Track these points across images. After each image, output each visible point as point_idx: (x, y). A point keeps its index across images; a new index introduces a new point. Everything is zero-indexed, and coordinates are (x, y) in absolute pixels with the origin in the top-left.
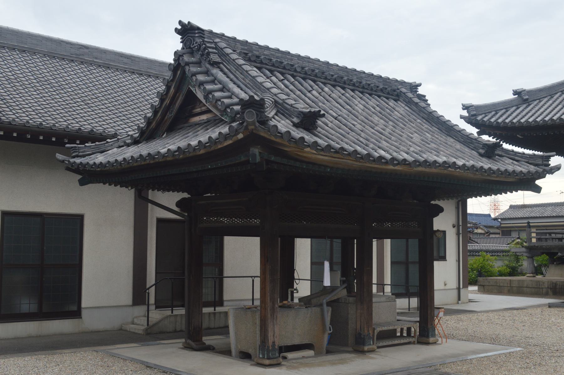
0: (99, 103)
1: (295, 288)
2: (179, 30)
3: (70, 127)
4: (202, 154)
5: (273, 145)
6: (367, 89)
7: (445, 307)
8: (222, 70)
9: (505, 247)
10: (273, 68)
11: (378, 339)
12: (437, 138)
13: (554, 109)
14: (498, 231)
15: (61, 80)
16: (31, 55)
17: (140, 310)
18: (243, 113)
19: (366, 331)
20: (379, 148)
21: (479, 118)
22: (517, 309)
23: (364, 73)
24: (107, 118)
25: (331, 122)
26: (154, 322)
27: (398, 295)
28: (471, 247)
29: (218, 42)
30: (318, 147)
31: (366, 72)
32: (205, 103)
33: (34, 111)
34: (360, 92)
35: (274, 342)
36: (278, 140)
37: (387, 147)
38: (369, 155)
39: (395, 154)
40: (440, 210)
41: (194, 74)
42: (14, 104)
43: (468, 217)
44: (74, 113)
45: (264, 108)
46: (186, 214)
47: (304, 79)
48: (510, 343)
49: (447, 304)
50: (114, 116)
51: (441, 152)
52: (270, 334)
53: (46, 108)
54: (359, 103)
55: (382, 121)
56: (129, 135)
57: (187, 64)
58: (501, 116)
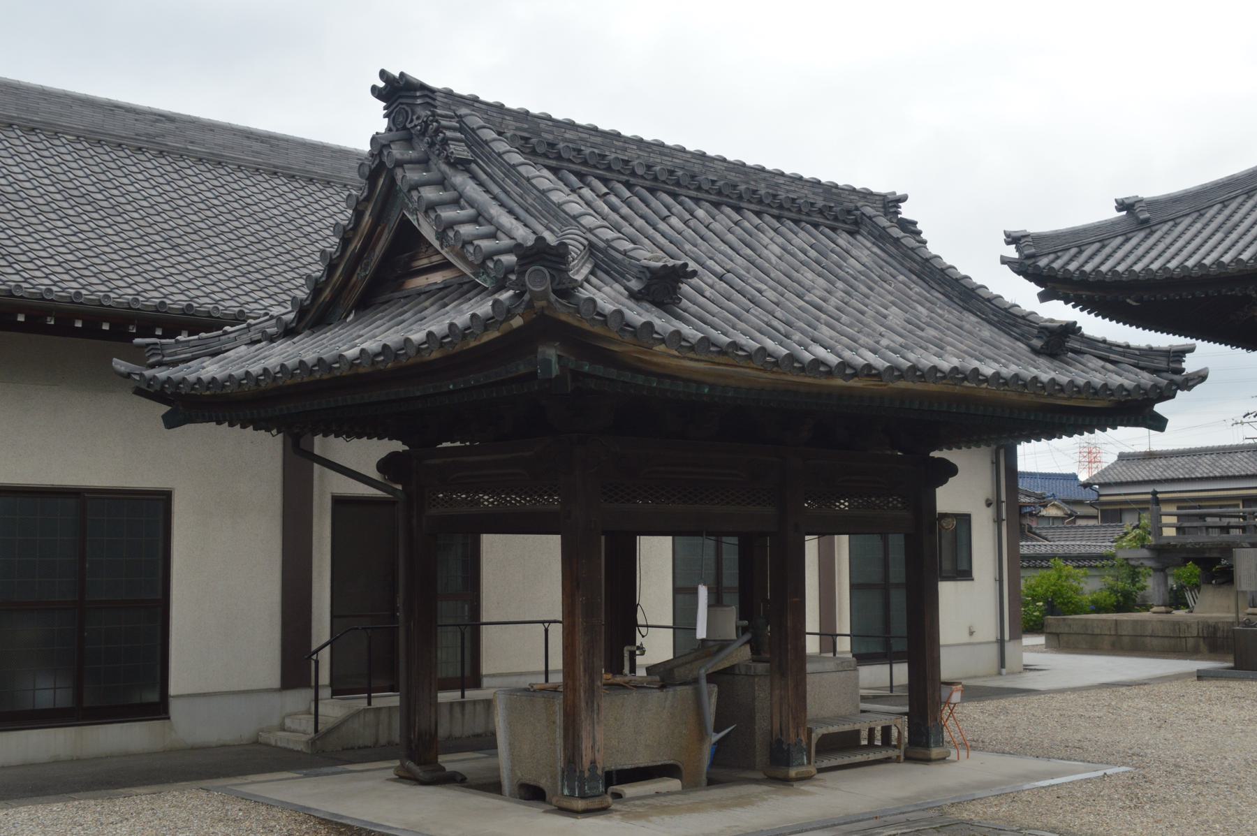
0: (203, 244)
1: (638, 644)
2: (380, 90)
3: (141, 299)
4: (436, 360)
5: (587, 339)
6: (789, 210)
7: (964, 682)
8: (474, 177)
9: (1103, 546)
10: (584, 169)
11: (818, 752)
12: (941, 316)
13: (1206, 242)
14: (1092, 511)
15: (115, 192)
16: (48, 138)
17: (299, 699)
18: (521, 274)
19: (792, 735)
20: (814, 340)
21: (1043, 262)
22: (1129, 685)
23: (782, 174)
24: (221, 277)
25: (712, 287)
26: (330, 726)
27: (863, 658)
28: (1026, 548)
29: (466, 115)
30: (683, 343)
31: (787, 172)
32: (439, 248)
33: (60, 264)
34: (773, 216)
35: (593, 762)
36: (597, 329)
37: (831, 338)
38: (792, 357)
39: (847, 354)
40: (949, 470)
41: (415, 187)
42: (16, 250)
44: (148, 267)
45: (566, 263)
46: (400, 487)
47: (652, 191)
49: (975, 677)
50: (236, 273)
51: (949, 348)
52: (586, 744)
53: (86, 257)
54: (773, 242)
55: (821, 281)
56: (272, 317)
57: (400, 164)
58: (1091, 257)
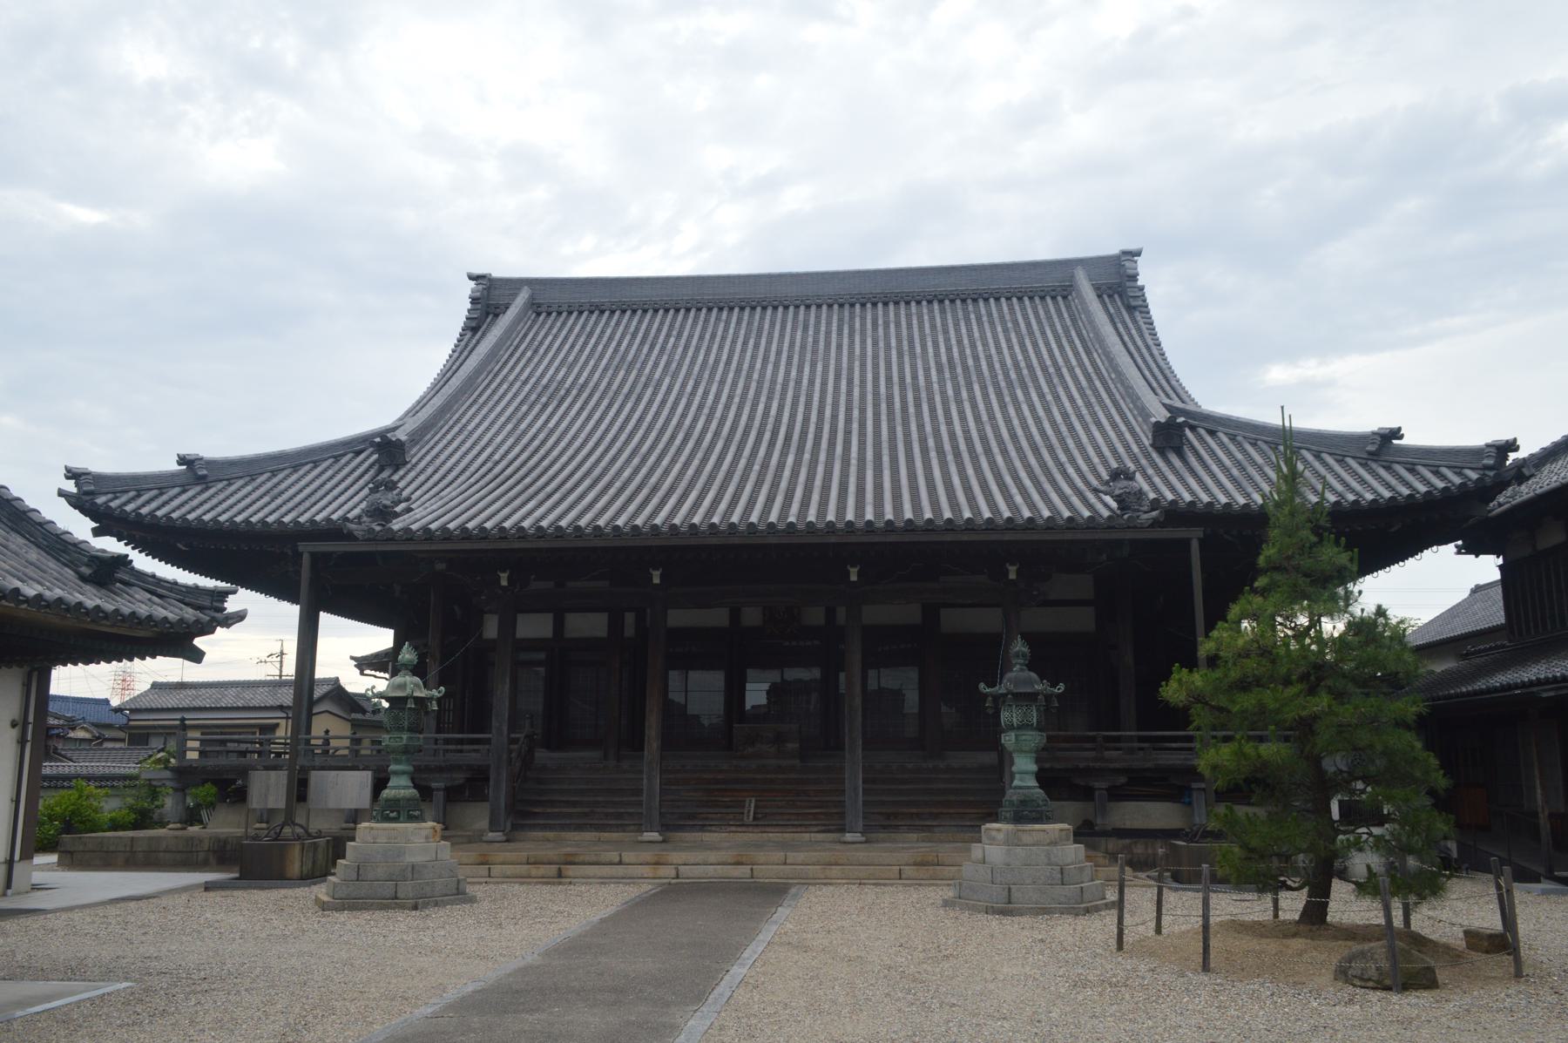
9: (130, 768)
14: (121, 735)
21: (100, 500)
28: (49, 768)
43: (51, 704)
48: (108, 974)
58: (148, 502)
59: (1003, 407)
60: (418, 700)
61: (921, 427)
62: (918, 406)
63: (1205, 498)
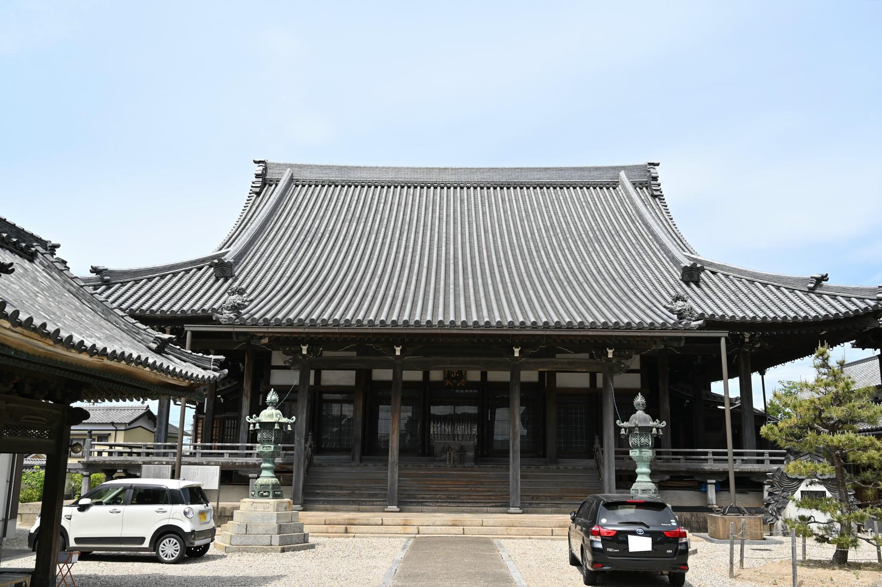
59: (589, 253)
60: (281, 424)
61: (543, 264)
62: (538, 251)
63: (823, 313)
